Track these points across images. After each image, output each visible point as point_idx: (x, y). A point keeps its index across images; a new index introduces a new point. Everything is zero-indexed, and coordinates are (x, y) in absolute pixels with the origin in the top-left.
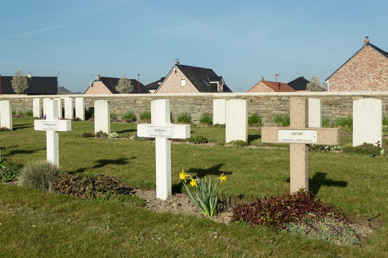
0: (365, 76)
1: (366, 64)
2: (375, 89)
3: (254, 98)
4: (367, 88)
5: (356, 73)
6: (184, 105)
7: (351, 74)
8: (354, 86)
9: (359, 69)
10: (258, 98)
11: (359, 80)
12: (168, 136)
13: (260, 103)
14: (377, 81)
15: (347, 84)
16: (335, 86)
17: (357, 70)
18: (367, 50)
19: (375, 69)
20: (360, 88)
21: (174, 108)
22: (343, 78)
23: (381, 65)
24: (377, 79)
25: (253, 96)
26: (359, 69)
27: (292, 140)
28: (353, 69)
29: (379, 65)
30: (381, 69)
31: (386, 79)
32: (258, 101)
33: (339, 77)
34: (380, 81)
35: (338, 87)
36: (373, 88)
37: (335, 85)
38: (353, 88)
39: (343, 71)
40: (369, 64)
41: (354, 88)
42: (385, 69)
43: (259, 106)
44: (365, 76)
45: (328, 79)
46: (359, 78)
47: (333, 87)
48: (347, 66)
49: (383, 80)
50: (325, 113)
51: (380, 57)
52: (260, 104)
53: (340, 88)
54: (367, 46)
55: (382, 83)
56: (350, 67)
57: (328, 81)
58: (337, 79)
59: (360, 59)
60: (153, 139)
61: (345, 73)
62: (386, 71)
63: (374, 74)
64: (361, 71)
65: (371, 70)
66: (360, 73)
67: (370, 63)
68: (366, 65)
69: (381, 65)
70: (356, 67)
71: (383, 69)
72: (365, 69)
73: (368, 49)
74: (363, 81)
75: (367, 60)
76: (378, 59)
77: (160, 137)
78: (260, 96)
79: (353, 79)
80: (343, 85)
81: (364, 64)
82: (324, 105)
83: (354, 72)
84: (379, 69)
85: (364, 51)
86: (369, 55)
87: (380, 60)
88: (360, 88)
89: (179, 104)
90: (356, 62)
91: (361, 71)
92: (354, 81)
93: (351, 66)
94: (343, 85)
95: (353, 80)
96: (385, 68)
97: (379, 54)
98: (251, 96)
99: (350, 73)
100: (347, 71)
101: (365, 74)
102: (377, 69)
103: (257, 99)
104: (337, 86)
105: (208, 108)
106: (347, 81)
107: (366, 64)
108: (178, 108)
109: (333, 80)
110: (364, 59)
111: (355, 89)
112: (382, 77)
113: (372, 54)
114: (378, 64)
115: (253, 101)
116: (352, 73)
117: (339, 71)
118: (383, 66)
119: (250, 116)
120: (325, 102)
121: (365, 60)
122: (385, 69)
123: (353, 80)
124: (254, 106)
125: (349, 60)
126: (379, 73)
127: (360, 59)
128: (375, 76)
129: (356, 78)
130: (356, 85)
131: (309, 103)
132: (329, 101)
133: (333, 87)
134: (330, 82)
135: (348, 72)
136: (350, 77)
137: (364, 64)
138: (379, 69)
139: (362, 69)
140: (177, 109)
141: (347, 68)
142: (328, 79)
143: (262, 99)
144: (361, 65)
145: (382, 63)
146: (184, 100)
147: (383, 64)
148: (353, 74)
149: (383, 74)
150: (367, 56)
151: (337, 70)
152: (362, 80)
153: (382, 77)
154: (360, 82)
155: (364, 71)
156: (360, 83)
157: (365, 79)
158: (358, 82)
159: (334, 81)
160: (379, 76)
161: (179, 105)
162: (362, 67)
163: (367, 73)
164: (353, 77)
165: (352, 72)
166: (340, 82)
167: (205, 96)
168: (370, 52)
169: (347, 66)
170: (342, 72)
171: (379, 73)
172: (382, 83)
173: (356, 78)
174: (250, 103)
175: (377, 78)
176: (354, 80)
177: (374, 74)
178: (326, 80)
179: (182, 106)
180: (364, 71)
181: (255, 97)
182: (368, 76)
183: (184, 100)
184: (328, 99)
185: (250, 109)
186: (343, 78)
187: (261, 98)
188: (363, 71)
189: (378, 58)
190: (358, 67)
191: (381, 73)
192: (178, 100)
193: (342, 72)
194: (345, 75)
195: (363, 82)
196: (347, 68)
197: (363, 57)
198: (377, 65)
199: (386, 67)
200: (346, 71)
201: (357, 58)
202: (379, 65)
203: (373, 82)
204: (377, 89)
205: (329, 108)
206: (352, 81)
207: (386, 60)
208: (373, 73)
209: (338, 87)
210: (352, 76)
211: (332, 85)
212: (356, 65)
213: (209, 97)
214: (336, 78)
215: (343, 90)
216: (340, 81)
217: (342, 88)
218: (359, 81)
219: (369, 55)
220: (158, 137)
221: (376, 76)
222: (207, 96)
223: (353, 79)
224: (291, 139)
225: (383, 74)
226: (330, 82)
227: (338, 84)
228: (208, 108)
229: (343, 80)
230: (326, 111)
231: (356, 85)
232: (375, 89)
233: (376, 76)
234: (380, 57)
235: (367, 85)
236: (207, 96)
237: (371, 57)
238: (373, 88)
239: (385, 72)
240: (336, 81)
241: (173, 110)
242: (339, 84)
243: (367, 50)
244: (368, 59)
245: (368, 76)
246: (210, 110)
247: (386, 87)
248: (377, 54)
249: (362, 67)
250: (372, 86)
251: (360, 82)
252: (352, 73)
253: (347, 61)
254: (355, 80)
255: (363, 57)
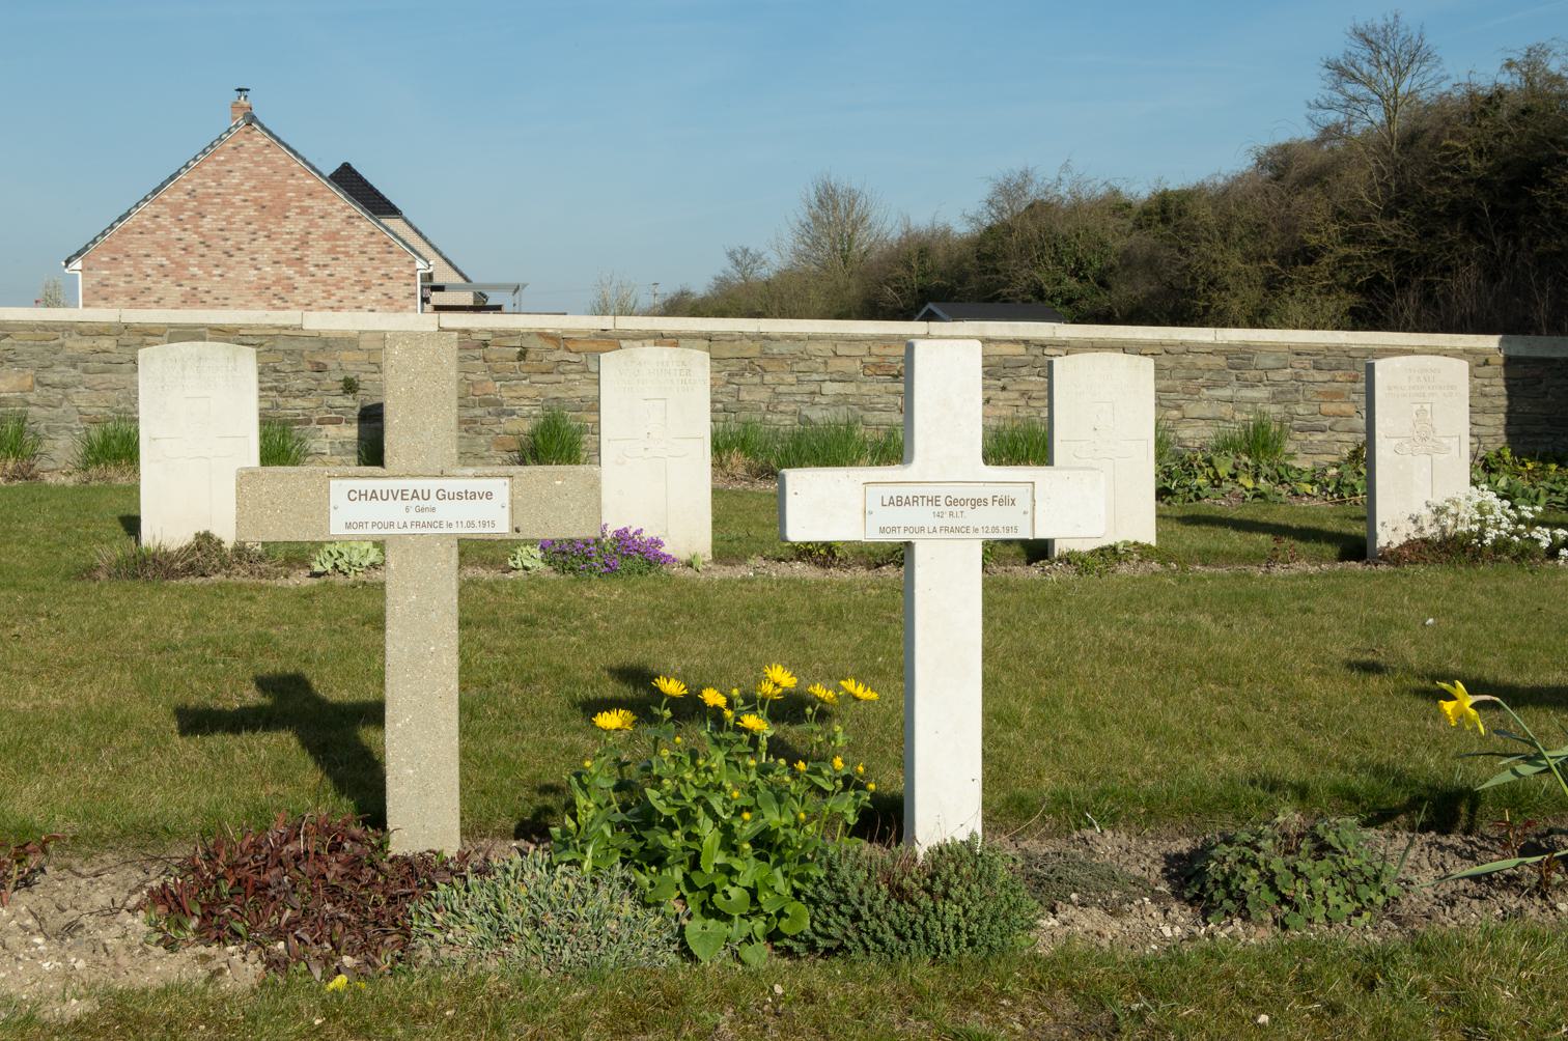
0: (240, 249)
1: (246, 201)
2: (283, 305)
3: (535, 344)
4: (251, 301)
5: (204, 236)
6: (109, 371)
7: (180, 239)
8: (195, 289)
9: (215, 220)
10: (557, 340)
11: (217, 266)
12: (995, 529)
13: (569, 368)
14: (290, 272)
15: (167, 282)
16: (110, 289)
17: (207, 223)
18: (247, 145)
19: (279, 224)
20: (222, 301)
21: (38, 389)
22: (147, 256)
23: (304, 211)
24: (290, 263)
25: (529, 334)
26: (215, 220)
27: (391, 524)
28: (190, 217)
29: (297, 207)
30: (303, 224)
31: (325, 266)
32: (559, 355)
33: (132, 248)
34: (302, 274)
35: (127, 293)
36: (275, 302)
37: (112, 282)
38: (191, 299)
39: (146, 223)
40: (255, 200)
41: (194, 299)
42: (321, 227)
43: (562, 378)
44: (240, 249)
45: (78, 254)
46: (214, 259)
47: (105, 292)
48: (162, 202)
49: (312, 269)
50: (874, 409)
51: (298, 179)
52: (570, 372)
53: (134, 299)
54: (248, 129)
55: (311, 282)
56: (178, 208)
57: (78, 264)
58: (120, 256)
59: (217, 177)
60: (900, 555)
61: (153, 232)
62: (325, 233)
63: (278, 244)
64: (221, 230)
65: (263, 228)
66: (218, 236)
67: (261, 197)
68: (247, 207)
69: (304, 211)
70: (201, 210)
71: (312, 224)
72: (241, 220)
73: (251, 139)
74: (233, 269)
75: (246, 186)
76: (292, 185)
77: (944, 535)
78: (568, 332)
79: (192, 261)
80: (148, 283)
81: (237, 199)
82: (870, 379)
83: (196, 233)
84: (295, 225)
85: (235, 148)
86: (257, 164)
87: (298, 189)
88: (222, 301)
89: (74, 366)
90: (200, 191)
91: (221, 230)
92: (194, 270)
93: (182, 205)
94: (148, 283)
95: (191, 265)
96: (321, 222)
97: (296, 165)
98: (519, 333)
99: (176, 232)
100: (165, 226)
101: (241, 243)
102: (289, 226)
103: (550, 346)
104: (119, 289)
105: (271, 389)
106: (162, 266)
107: (246, 201)
108: (65, 386)
109: (103, 259)
110: (234, 178)
111: (199, 305)
112: (307, 256)
113: (267, 162)
114: (293, 204)
115: (531, 356)
116: (183, 235)
117: (127, 222)
118: (312, 214)
119: (993, 423)
120: (874, 364)
121: (238, 184)
122: (321, 227)
123: (191, 265)
124: (536, 378)
125: (172, 178)
126: (296, 240)
127: (217, 177)
128: (279, 251)
129: (203, 256)
130: (203, 286)
131: (1378, 374)
132: (892, 360)
133: (105, 292)
134: (90, 269)
135: (169, 232)
136: (177, 253)
137: (237, 199)
138: (295, 225)
139: (227, 219)
140: (56, 395)
141: (165, 213)
142: (78, 254)
143: (581, 346)
144: (224, 203)
145: (308, 202)
146: (106, 343)
147: (312, 207)
148: (192, 238)
149: (312, 246)
150: (246, 168)
151: (120, 219)
152: (230, 268)
153: (307, 256)
154: (221, 276)
155: (237, 230)
156: (219, 279)
157: (242, 262)
158: (211, 275)
159: (107, 265)
160: (297, 254)
161: (73, 372)
162: (229, 211)
163: (247, 239)
164: (191, 253)
165: (185, 230)
166: (135, 273)
167: (250, 327)
168: (259, 152)
169: (162, 202)
170: (140, 227)
171: (296, 240)
172: (311, 282)
173: (203, 256)
174: (517, 364)
175: (288, 259)
176: (195, 266)
177: (278, 244)
178: (68, 262)
179: (98, 378)
180: (237, 230)
181: (542, 335)
182: (253, 253)
183: (106, 343)
184: (888, 351)
185: (513, 394)
186: (147, 256)
187: (575, 341)
188: (231, 230)
189: (293, 182)
190: (211, 213)
191: (304, 243)
192: (69, 343)
193: (140, 227)
194: (154, 243)
195: (231, 275)
196: (165, 213)
197: (231, 171)
198: (286, 207)
199: (322, 217)
200: (160, 227)
201: (206, 175)
202: (297, 207)
203: (273, 275)
204: (288, 304)
205: (893, 390)
206: (185, 267)
207: (324, 191)
208: (274, 240)
209: (127, 293)
210: (184, 249)
211: (99, 283)
212: (201, 204)
213: (276, 332)
214: (116, 252)
215: (149, 305)
216: (135, 266)
217: (142, 299)
218: (218, 271)
219: (257, 164)
220: (934, 535)
221: (284, 253)
222: (264, 327)
223: (192, 261)
224: (386, 520)
225: (312, 246)
226: (85, 269)
227: (123, 279)
228: (271, 389)
229: (149, 261)
230: (876, 400)
231: (203, 286)
232: (283, 305)
233: (284, 253)
234: (298, 179)
235: (249, 288)
236: (258, 327)
237: (264, 175)
238: (275, 302)
239: (320, 236)
240: (117, 268)
241: (32, 397)
242: (129, 279)
243: (247, 145)
244: (253, 183)
245: (253, 253)
246: (280, 400)
247: (324, 298)
248: (289, 165)
249: (229, 211)
250: (271, 292)
251: (221, 276)
252: (183, 235)
253: (163, 185)
254: (200, 266)
255: (231, 171)
